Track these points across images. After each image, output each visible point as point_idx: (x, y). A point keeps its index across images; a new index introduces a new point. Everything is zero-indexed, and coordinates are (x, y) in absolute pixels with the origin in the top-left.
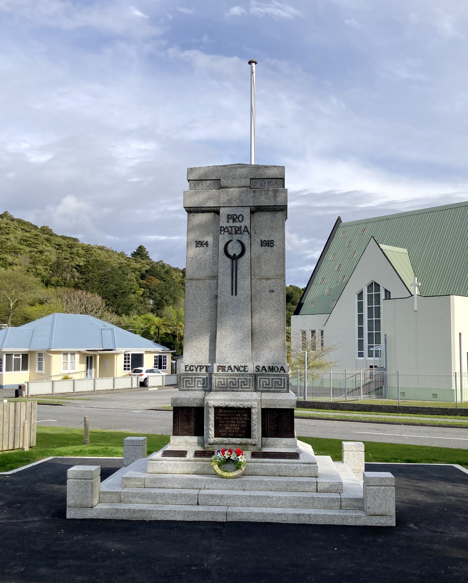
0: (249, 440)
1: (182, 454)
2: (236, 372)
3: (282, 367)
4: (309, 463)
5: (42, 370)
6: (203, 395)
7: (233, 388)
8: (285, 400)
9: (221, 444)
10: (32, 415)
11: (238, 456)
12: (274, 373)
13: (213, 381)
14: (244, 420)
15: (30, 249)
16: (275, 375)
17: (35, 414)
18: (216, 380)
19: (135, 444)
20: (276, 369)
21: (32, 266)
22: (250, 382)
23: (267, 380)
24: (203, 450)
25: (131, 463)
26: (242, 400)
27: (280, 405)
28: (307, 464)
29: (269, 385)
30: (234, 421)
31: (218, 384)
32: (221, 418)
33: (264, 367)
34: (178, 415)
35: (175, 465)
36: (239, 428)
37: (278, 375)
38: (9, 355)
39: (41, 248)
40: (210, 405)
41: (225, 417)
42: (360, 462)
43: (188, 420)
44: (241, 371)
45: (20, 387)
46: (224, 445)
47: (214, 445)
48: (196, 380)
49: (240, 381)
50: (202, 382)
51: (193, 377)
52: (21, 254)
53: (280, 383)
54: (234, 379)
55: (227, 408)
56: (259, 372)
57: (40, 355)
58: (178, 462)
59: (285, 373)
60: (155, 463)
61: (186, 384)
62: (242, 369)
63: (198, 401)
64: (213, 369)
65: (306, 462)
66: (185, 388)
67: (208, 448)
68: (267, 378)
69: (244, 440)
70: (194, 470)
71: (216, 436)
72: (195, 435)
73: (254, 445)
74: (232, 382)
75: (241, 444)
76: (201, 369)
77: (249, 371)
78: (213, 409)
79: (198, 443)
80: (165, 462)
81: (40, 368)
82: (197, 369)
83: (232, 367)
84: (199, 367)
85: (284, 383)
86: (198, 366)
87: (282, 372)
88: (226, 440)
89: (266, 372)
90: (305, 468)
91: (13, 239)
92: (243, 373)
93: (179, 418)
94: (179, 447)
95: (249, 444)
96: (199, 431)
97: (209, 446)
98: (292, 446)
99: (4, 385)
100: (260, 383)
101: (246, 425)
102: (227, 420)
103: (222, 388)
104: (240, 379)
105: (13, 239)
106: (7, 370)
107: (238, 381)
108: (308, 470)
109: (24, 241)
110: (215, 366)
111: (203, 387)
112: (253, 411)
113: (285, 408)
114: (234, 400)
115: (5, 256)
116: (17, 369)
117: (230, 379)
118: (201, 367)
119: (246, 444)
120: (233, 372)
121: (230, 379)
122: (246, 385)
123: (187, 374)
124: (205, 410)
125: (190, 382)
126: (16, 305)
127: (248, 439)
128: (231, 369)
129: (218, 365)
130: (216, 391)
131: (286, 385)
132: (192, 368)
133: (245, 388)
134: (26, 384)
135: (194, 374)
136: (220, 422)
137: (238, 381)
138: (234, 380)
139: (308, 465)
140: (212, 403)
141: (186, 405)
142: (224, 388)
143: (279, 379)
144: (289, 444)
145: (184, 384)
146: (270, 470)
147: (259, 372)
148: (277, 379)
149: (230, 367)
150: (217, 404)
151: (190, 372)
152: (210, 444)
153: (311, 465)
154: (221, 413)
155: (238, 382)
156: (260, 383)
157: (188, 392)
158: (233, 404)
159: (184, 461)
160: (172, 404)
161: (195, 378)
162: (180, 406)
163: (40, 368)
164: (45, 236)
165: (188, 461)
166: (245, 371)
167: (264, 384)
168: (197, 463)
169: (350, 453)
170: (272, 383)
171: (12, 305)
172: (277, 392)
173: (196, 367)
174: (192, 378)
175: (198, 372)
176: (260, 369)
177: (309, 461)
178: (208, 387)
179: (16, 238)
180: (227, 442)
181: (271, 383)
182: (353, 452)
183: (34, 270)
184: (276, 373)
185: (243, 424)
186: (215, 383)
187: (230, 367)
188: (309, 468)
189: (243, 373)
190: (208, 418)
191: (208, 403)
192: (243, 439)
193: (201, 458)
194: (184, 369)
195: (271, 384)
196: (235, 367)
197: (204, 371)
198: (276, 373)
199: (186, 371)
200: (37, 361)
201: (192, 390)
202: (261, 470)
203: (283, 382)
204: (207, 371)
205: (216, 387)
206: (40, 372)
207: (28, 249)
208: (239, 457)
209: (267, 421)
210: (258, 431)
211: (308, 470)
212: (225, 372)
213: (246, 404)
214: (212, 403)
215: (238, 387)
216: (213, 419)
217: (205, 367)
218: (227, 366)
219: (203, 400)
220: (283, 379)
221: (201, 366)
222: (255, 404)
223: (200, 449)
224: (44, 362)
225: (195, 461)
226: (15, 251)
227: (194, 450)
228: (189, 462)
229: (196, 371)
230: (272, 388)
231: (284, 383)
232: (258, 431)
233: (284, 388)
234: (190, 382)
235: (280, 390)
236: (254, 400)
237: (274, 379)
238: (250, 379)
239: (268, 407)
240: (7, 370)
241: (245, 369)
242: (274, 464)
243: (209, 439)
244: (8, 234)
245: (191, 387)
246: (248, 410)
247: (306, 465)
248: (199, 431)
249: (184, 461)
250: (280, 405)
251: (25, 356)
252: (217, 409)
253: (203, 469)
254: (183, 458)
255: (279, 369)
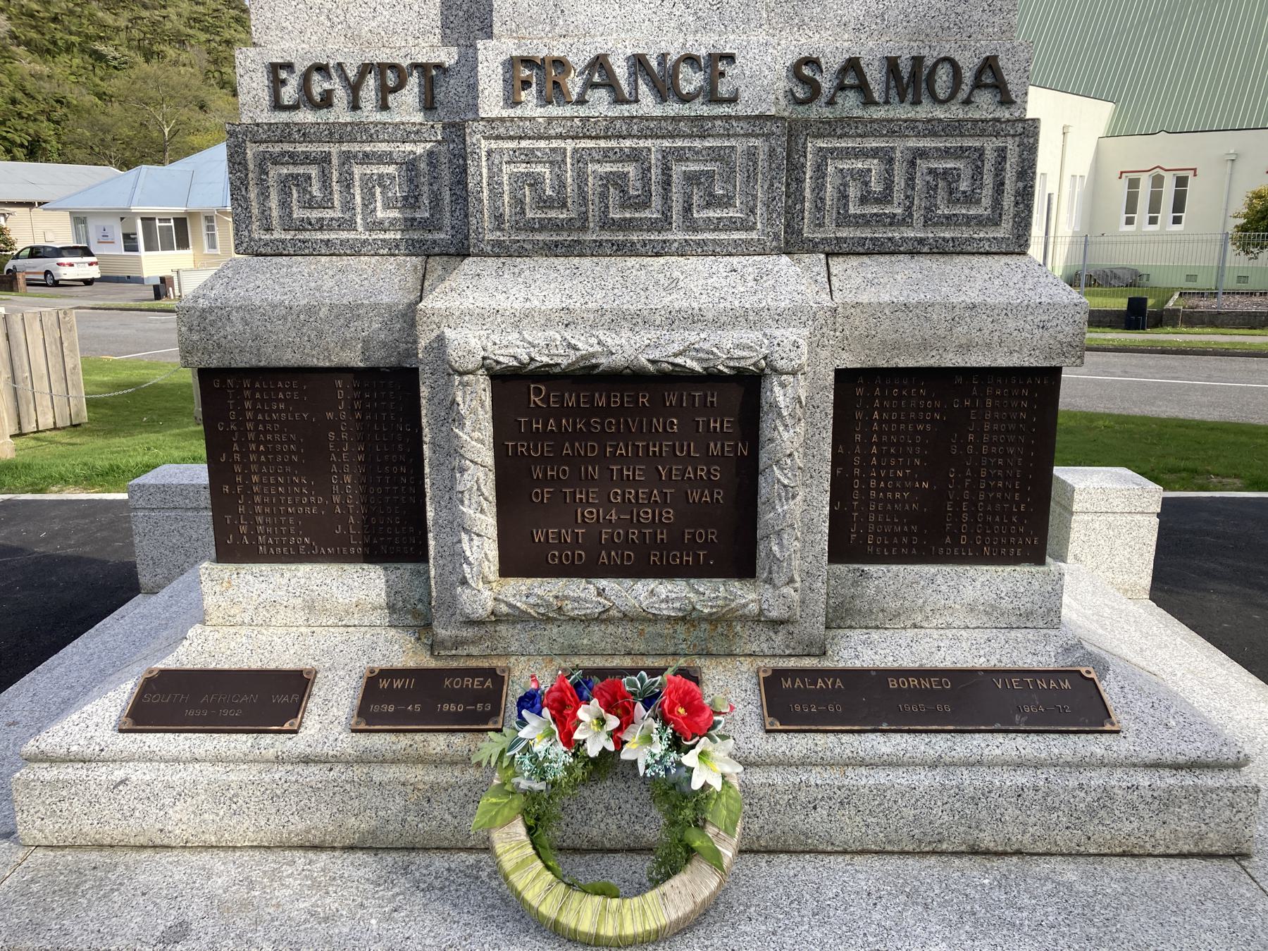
0: (743, 595)
1: (266, 699)
2: (648, 104)
3: (990, 65)
4: (1193, 766)
5: (215, 247)
6: (412, 281)
7: (625, 225)
8: (1009, 310)
9: (548, 620)
10: (65, 345)
11: (677, 744)
12: (925, 111)
13: (479, 172)
14: (709, 459)
15: (208, 36)
16: (932, 128)
17: (72, 344)
18: (494, 169)
19: (179, 501)
20: (943, 77)
21: (213, 68)
22: (750, 178)
23: (874, 165)
24: (432, 664)
25: (169, 580)
26: (694, 319)
27: (966, 348)
28: (1177, 767)
29: (885, 198)
30: (634, 460)
31: (519, 202)
32: (545, 448)
33: (853, 65)
34: (241, 424)
35: (222, 794)
36: (669, 514)
37: (954, 128)
38: (148, 221)
39: (227, 34)
40: (453, 354)
41: (576, 436)
42: (1135, 558)
43: (314, 460)
44: (685, 99)
45: (163, 280)
46: (568, 628)
47: (502, 628)
48: (357, 171)
49: (678, 170)
50: (397, 191)
51: (334, 149)
52: (192, 46)
53: (964, 186)
54: (635, 156)
55: (587, 379)
56: (818, 111)
57: (209, 219)
58: (238, 775)
59: (1004, 114)
60: (66, 784)
61: (285, 204)
62: (691, 80)
63: (372, 326)
64: (473, 87)
65: (1168, 757)
66: (278, 235)
67: (458, 643)
68: (875, 153)
69: (708, 593)
70: (357, 824)
71: (508, 568)
72: (372, 555)
73: (776, 624)
74: (619, 181)
75: (688, 618)
76: (385, 91)
77: (745, 95)
78: (482, 385)
79: (392, 608)
80: (139, 773)
81: (213, 245)
82: (354, 89)
83: (621, 71)
84: (371, 81)
85: (999, 186)
86: (365, 69)
87: (986, 107)
88: (581, 593)
89: (869, 101)
90: (1166, 801)
91: (174, 17)
92: (699, 108)
93: (244, 444)
94: (265, 635)
95: (744, 619)
96: (392, 530)
97: (468, 633)
98: (1029, 614)
99: (145, 276)
100: (819, 188)
101: (719, 495)
102: (587, 460)
103: (544, 226)
104: (681, 155)
105: (174, 17)
106: (147, 249)
107: (666, 170)
108: (1185, 810)
109: (195, 20)
110: (491, 59)
111: (410, 224)
112: (779, 394)
113: (1002, 362)
114: (638, 320)
115: (162, 47)
116: (167, 246)
117: (606, 155)
118: (389, 77)
119: (722, 621)
120: (625, 110)
121: (606, 155)
122: (726, 202)
123: (285, 133)
124: (424, 391)
125: (316, 190)
126: (174, 133)
127: (736, 586)
128: (611, 84)
129: (510, 48)
130: (502, 251)
131: (1008, 201)
132: (319, 85)
133: (717, 226)
134: (175, 275)
135: (335, 133)
136: (537, 473)
137: (666, 170)
138: (631, 169)
139: (1189, 780)
140: (470, 342)
141: (289, 358)
142: (557, 227)
143: (959, 153)
144: (1005, 604)
145: (274, 203)
146: (909, 813)
147: (818, 111)
148: (947, 153)
149: (600, 63)
150: (513, 348)
151: (305, 116)
152: (471, 623)
153: (1209, 780)
154: (545, 414)
155: (667, 183)
156: (819, 188)
157: (302, 265)
158: (626, 348)
159: (279, 760)
160: (187, 351)
161: (347, 158)
162: (242, 361)
163: (213, 245)
164: (233, 12)
165: (306, 760)
166: (713, 98)
167: (853, 192)
168: (378, 774)
169: (1099, 523)
170: (911, 180)
171: (166, 131)
172: (941, 250)
173: (352, 73)
174: (326, 159)
175: (369, 113)
176: (826, 84)
177: (1191, 751)
178: (442, 227)
179: (179, 15)
180: (592, 609)
181: (899, 181)
182: (1111, 518)
183: (217, 74)
184: (940, 113)
185: (698, 482)
186: (496, 195)
187: (600, 63)
188: (1194, 796)
189: (699, 108)
190: (452, 452)
191: (441, 339)
192: (704, 585)
193: (404, 741)
194: (265, 97)
195: (898, 196)
196: (638, 63)
197: (409, 97)
198: (940, 113)
199: (277, 105)
200: (204, 231)
201: (331, 250)
202: (844, 816)
203: (988, 179)
204: (429, 104)
205: (499, 218)
206: (213, 251)
207: (203, 37)
208: (690, 759)
209: (866, 457)
210: (809, 527)
211: (1185, 810)
212: (568, 111)
213: (730, 347)
214: (470, 342)
215: (665, 222)
216: (489, 458)
217: (414, 80)
218: (579, 59)
219: (409, 317)
220: (990, 155)
221: (382, 68)
222: (790, 344)
223: (401, 652)
224: (217, 233)
225: (363, 759)
226: (180, 40)
227: (362, 665)
228: (314, 773)
229: (355, 106)
230: (905, 221)
231: (999, 186)
232: (809, 527)
233: (995, 222)
234: (316, 190)
235: (966, 233)
236: (780, 317)
237: (923, 153)
238: (751, 154)
239: (881, 363)
240: (147, 249)
241: (714, 77)
242: (938, 776)
243: (464, 594)
244: (164, 7)
245: (321, 226)
246: (743, 390)
247: (1169, 779)
248: (392, 530)
249: (279, 760)
250: (966, 348)
251: (181, 222)
252: (510, 384)
253: (422, 814)
254: (270, 744)
255: (968, 76)
